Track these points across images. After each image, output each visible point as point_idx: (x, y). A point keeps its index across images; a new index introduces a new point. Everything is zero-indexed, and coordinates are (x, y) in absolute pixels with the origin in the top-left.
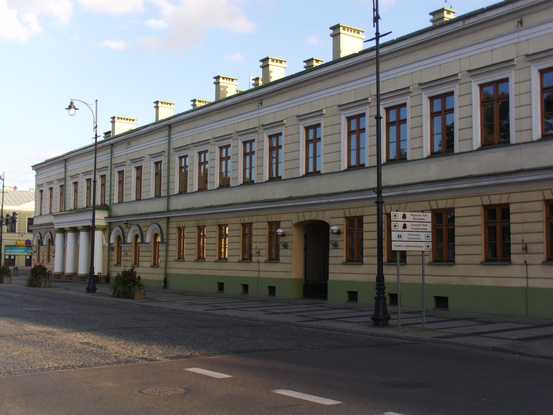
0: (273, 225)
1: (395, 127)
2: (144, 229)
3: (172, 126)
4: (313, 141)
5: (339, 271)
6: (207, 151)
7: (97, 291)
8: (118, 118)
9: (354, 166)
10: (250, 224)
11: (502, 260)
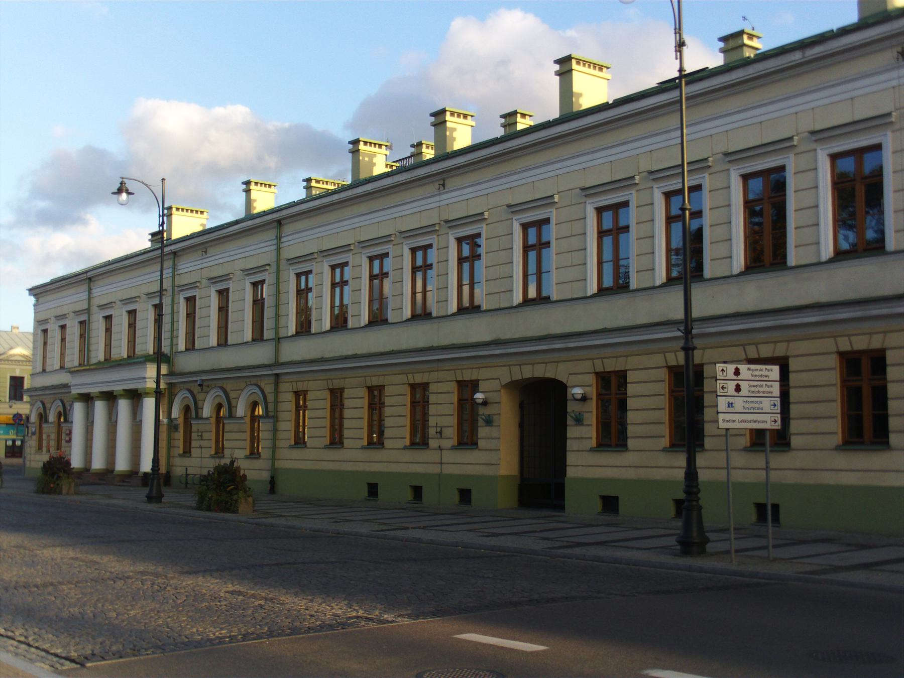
0: (468, 387)
2: (232, 395)
3: (283, 222)
4: (536, 247)
5: (585, 462)
6: (346, 264)
7: (163, 500)
8: (178, 209)
10: (425, 386)
11: (872, 443)
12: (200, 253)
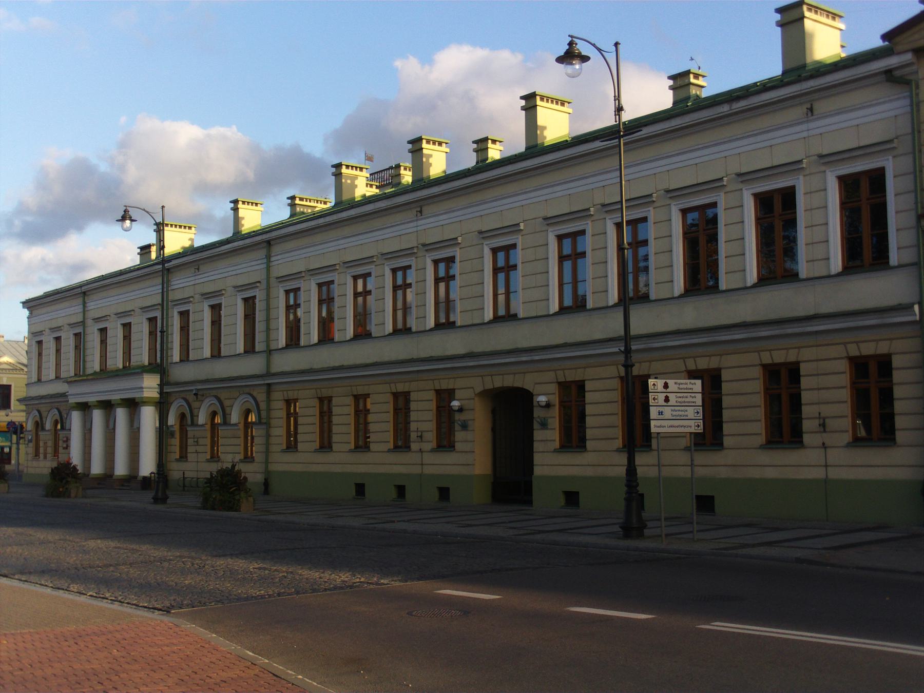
0: (444, 396)
1: (570, 262)
2: (227, 403)
3: (272, 243)
4: (504, 271)
5: (550, 462)
7: (169, 501)
9: (502, 317)
10: (406, 395)
12: (193, 270)
